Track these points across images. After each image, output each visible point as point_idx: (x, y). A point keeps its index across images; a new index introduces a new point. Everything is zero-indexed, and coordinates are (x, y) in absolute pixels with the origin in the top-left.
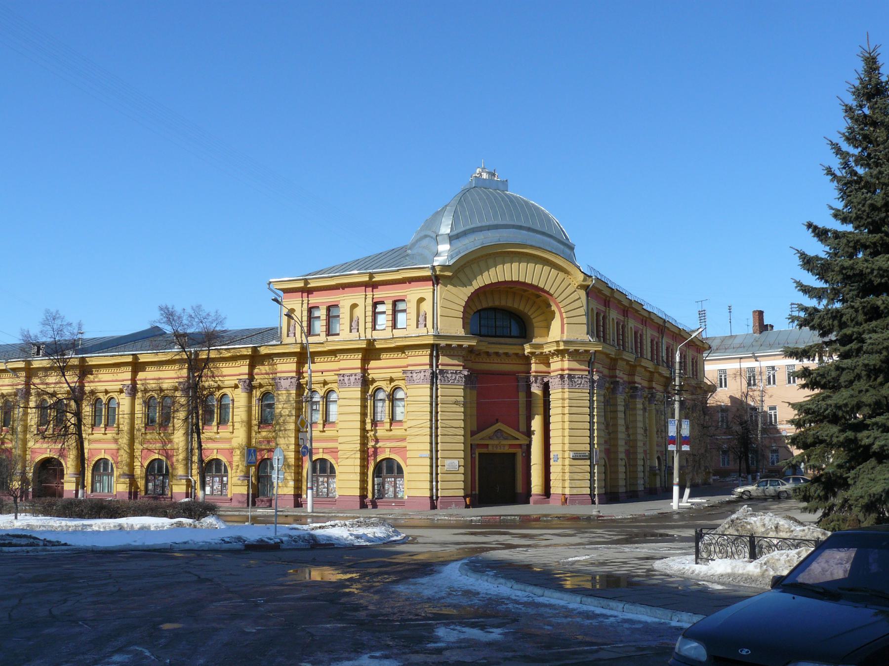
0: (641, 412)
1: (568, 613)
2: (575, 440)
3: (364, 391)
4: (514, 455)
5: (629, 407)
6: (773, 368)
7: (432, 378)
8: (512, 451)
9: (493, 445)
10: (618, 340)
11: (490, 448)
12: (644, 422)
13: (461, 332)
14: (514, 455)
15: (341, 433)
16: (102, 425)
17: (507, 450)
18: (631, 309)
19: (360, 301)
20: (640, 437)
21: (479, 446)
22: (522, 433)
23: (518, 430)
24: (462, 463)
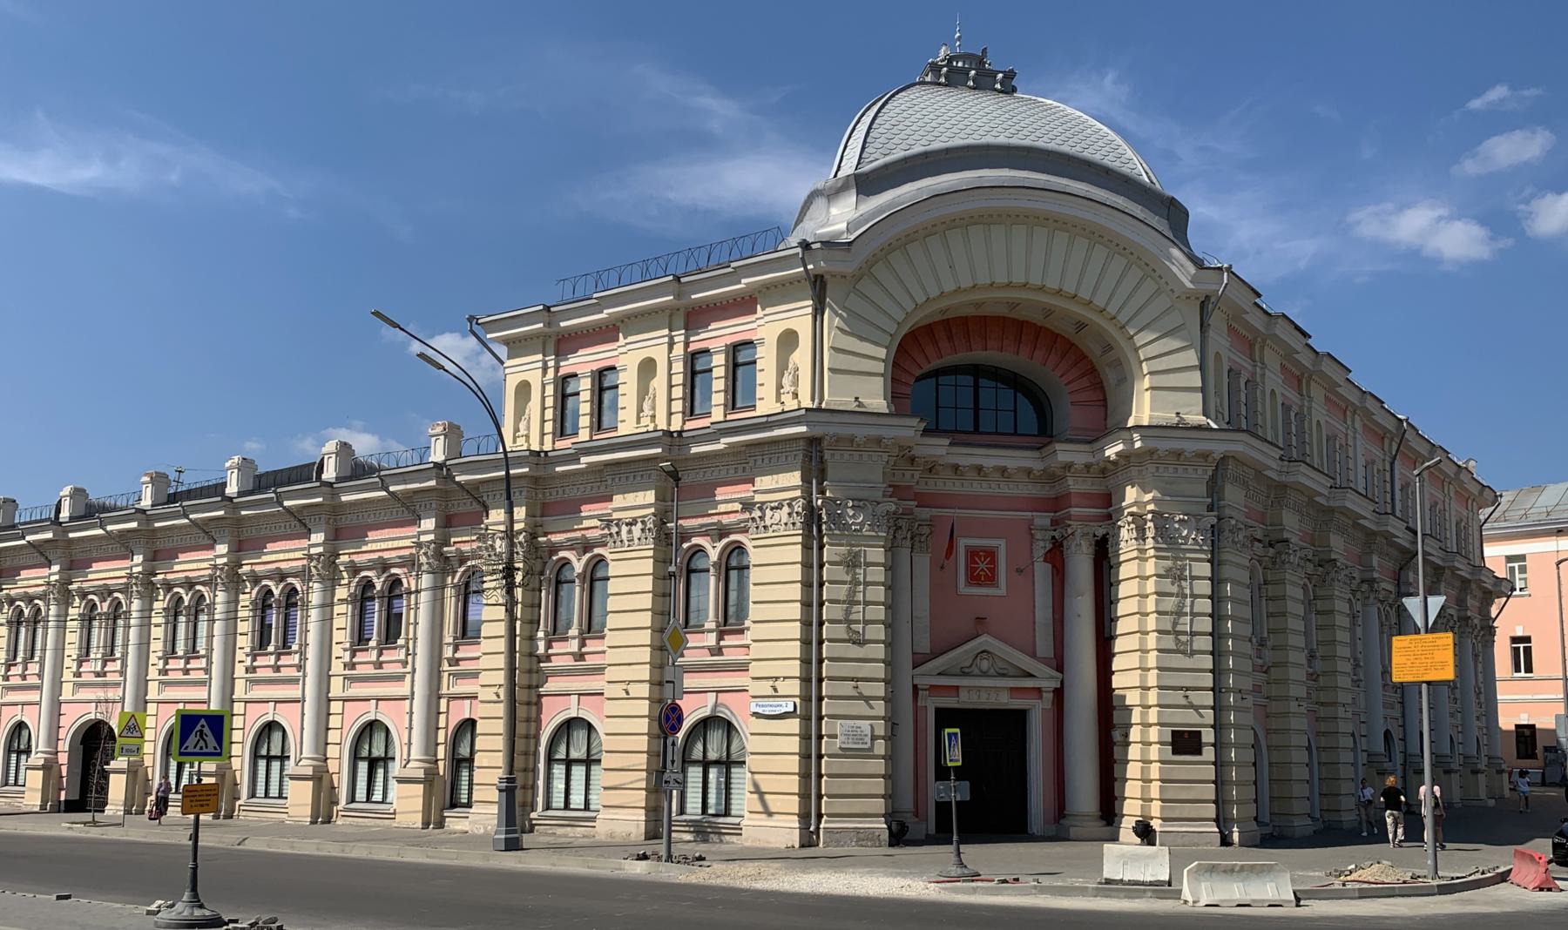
0: (1344, 621)
1: (1176, 640)
2: (1177, 791)
3: (661, 561)
4: (1021, 717)
5: (1316, 603)
6: (1522, 558)
7: (807, 525)
8: (1017, 704)
9: (969, 689)
10: (1287, 423)
11: (964, 696)
12: (1353, 645)
13: (877, 401)
14: (1021, 717)
15: (757, 651)
16: (574, 632)
17: (1005, 701)
18: (1312, 371)
19: (660, 354)
20: (1344, 681)
21: (934, 689)
22: (1045, 661)
23: (1033, 655)
24: (880, 731)
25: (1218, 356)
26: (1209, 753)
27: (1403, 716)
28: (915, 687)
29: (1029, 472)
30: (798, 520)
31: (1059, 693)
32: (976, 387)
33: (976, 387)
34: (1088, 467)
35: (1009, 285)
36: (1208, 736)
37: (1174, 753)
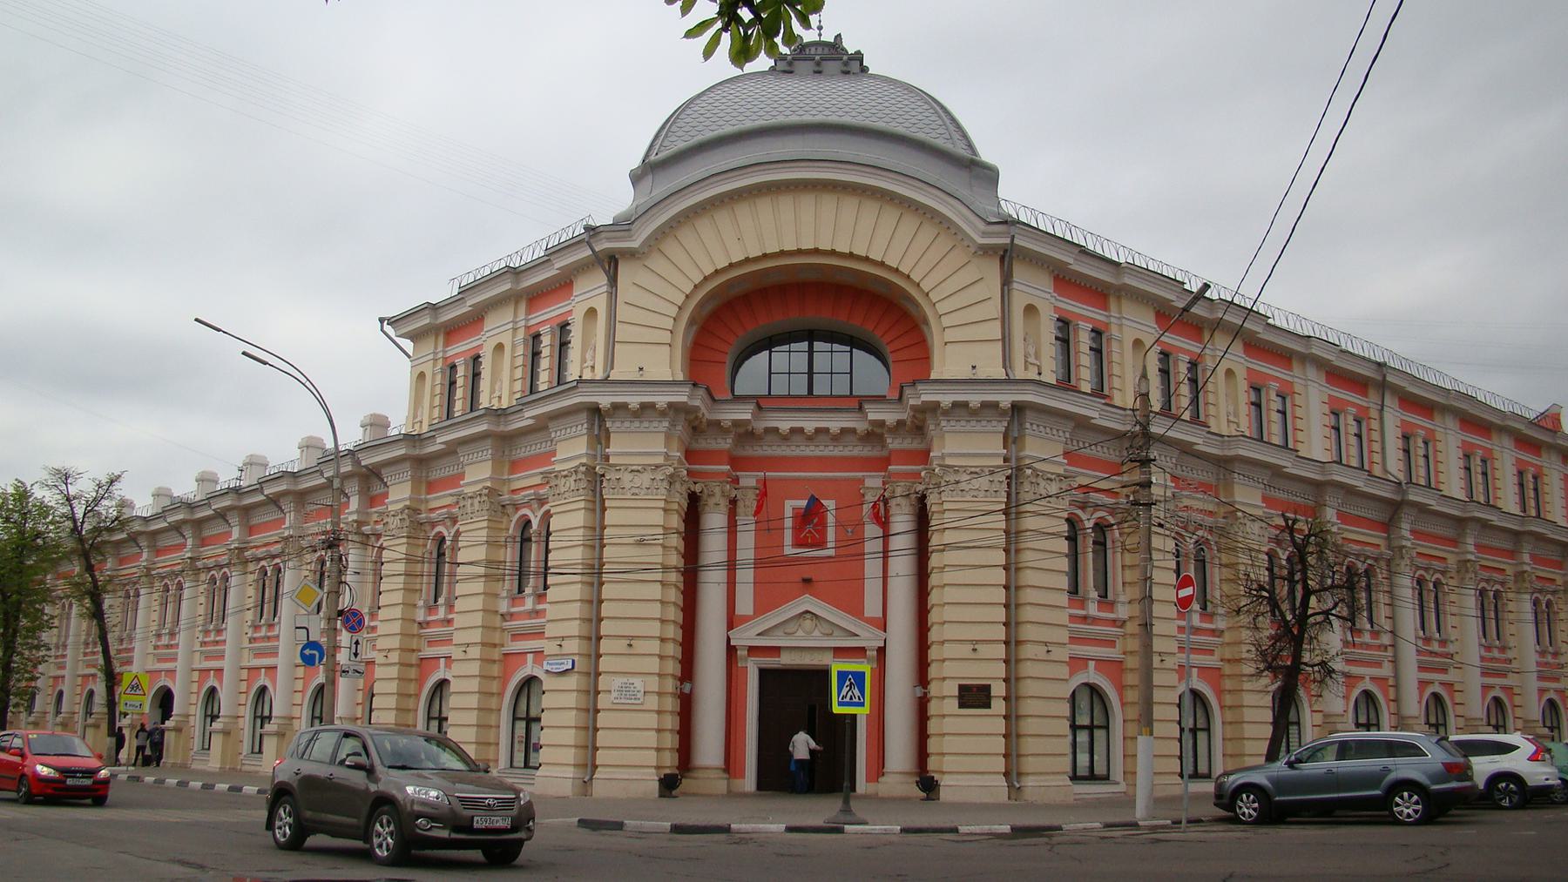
21: (753, 650)
22: (871, 621)
25: (1030, 310)
26: (998, 706)
27: (1396, 677)
28: (731, 650)
29: (853, 431)
30: (583, 484)
31: (882, 651)
32: (811, 352)
33: (811, 352)
34: (900, 423)
35: (731, 265)
36: (998, 689)
37: (961, 706)
